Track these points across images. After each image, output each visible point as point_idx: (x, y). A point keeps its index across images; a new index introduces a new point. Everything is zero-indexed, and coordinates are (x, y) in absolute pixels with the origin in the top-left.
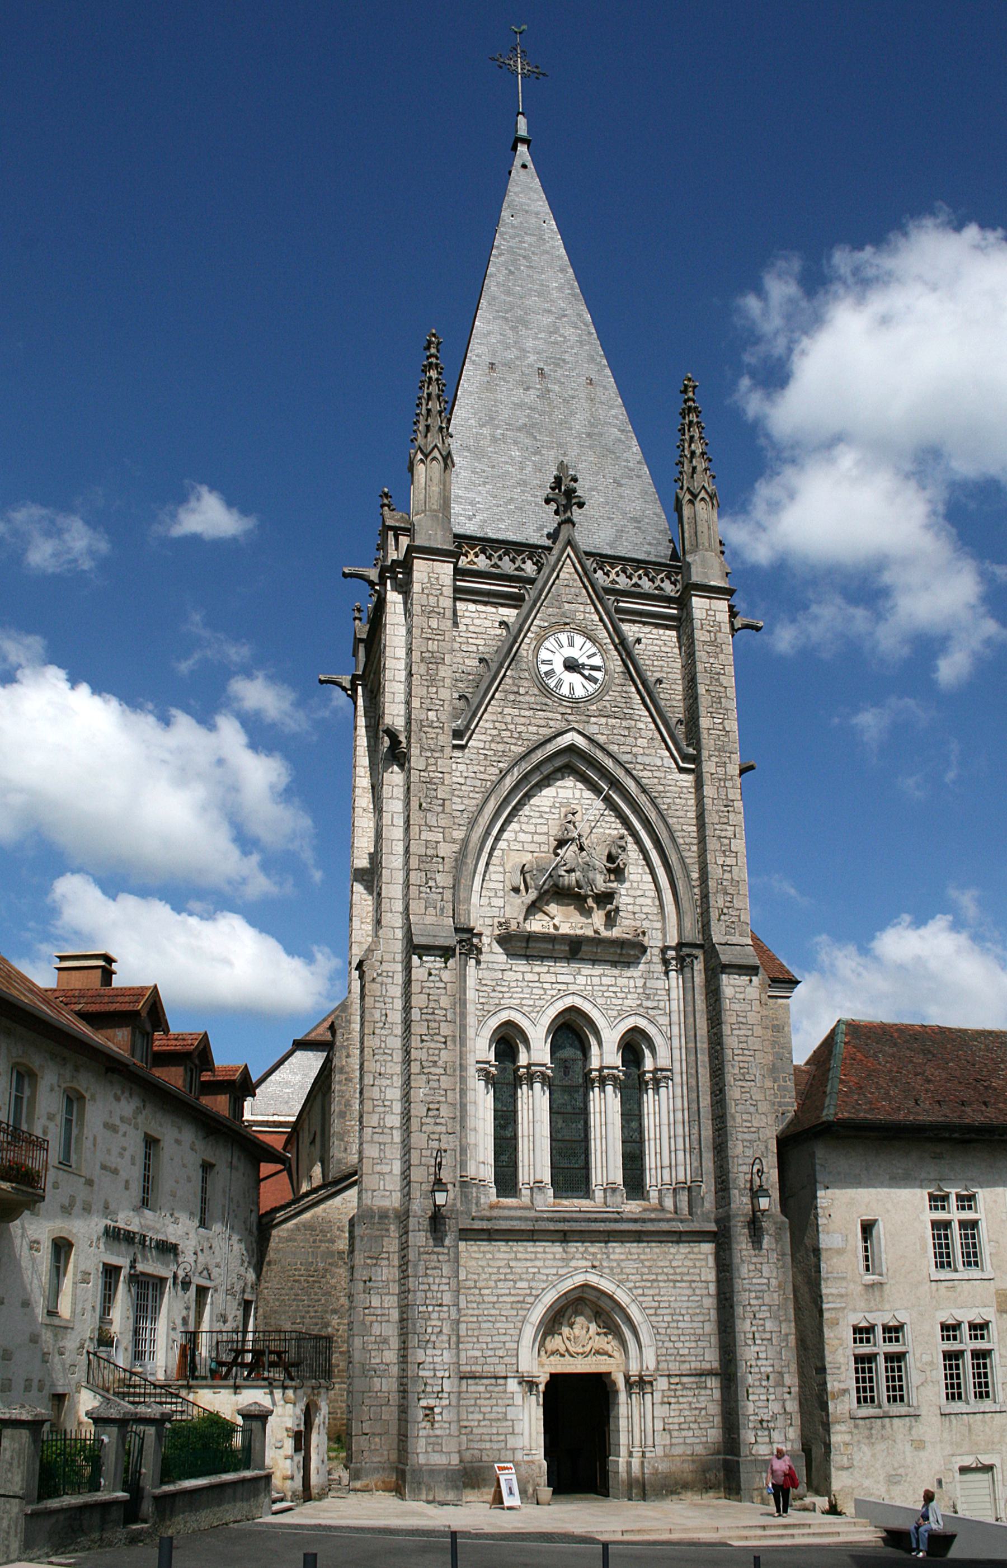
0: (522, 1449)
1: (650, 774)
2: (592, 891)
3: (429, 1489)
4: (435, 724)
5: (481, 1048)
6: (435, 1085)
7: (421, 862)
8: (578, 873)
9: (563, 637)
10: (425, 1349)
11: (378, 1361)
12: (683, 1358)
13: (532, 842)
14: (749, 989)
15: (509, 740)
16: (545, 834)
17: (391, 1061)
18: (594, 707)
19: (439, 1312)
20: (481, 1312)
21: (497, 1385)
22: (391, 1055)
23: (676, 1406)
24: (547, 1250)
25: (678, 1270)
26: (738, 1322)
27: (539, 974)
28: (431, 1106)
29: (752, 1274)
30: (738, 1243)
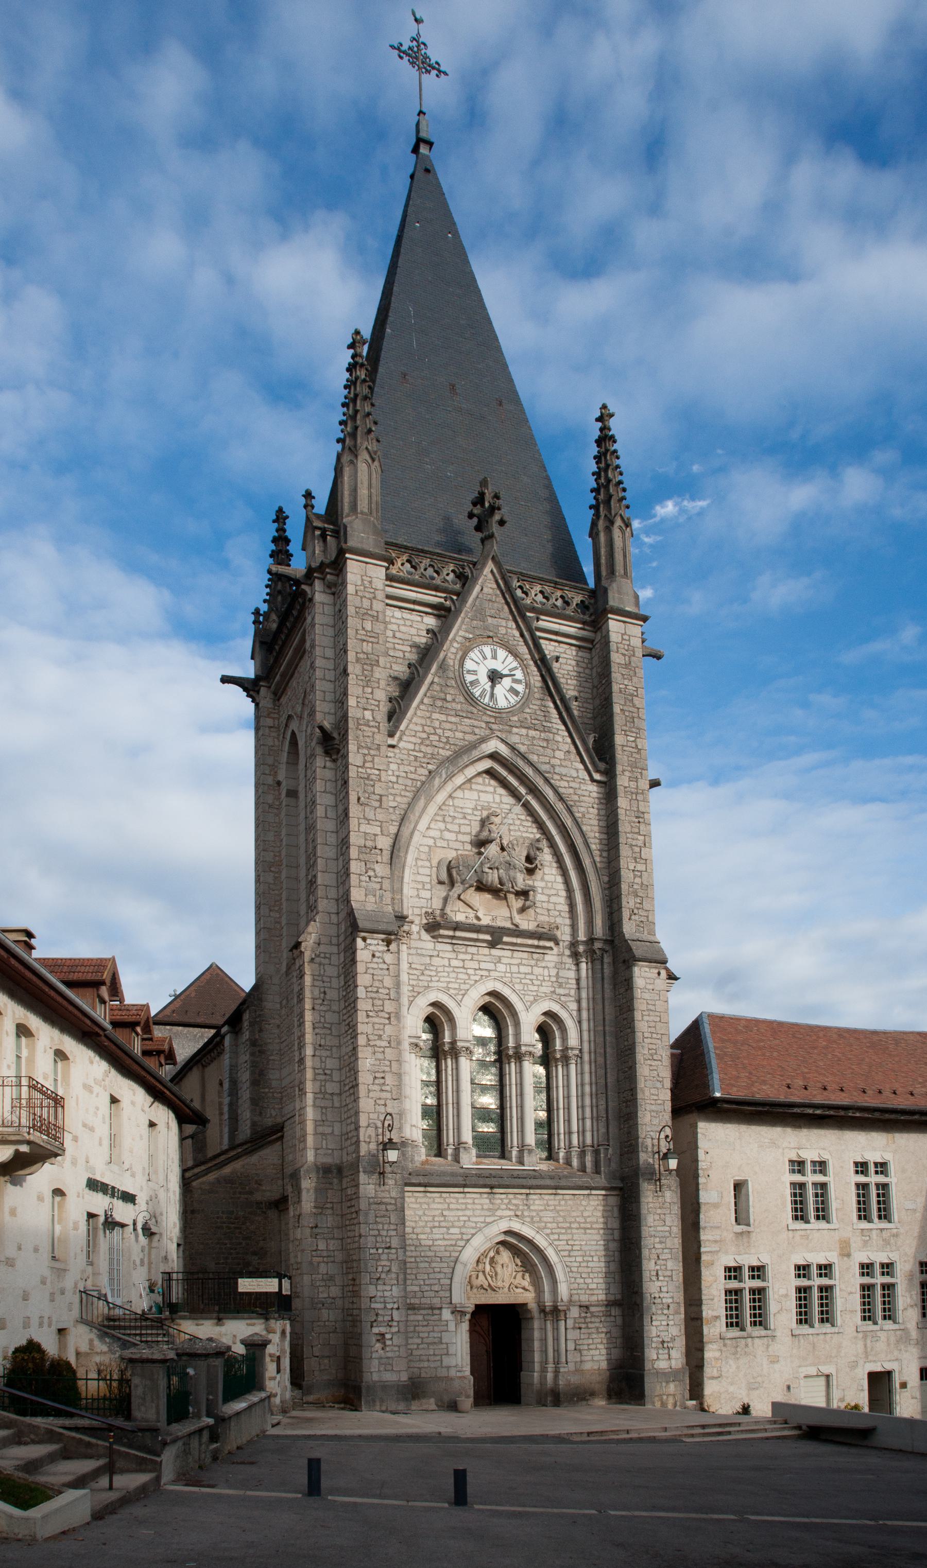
0: (456, 1366)
1: (566, 784)
2: (513, 887)
3: (382, 1401)
4: (372, 724)
5: (413, 1025)
6: (380, 1056)
7: (360, 852)
9: (487, 650)
10: (376, 1285)
11: (326, 1295)
13: (456, 840)
14: (657, 981)
16: (467, 834)
18: (516, 718)
20: (418, 1254)
21: (433, 1315)
22: (330, 1029)
24: (476, 1201)
25: (588, 1220)
26: (644, 1262)
27: (463, 961)
28: (377, 1075)
29: (656, 1223)
30: (647, 1197)
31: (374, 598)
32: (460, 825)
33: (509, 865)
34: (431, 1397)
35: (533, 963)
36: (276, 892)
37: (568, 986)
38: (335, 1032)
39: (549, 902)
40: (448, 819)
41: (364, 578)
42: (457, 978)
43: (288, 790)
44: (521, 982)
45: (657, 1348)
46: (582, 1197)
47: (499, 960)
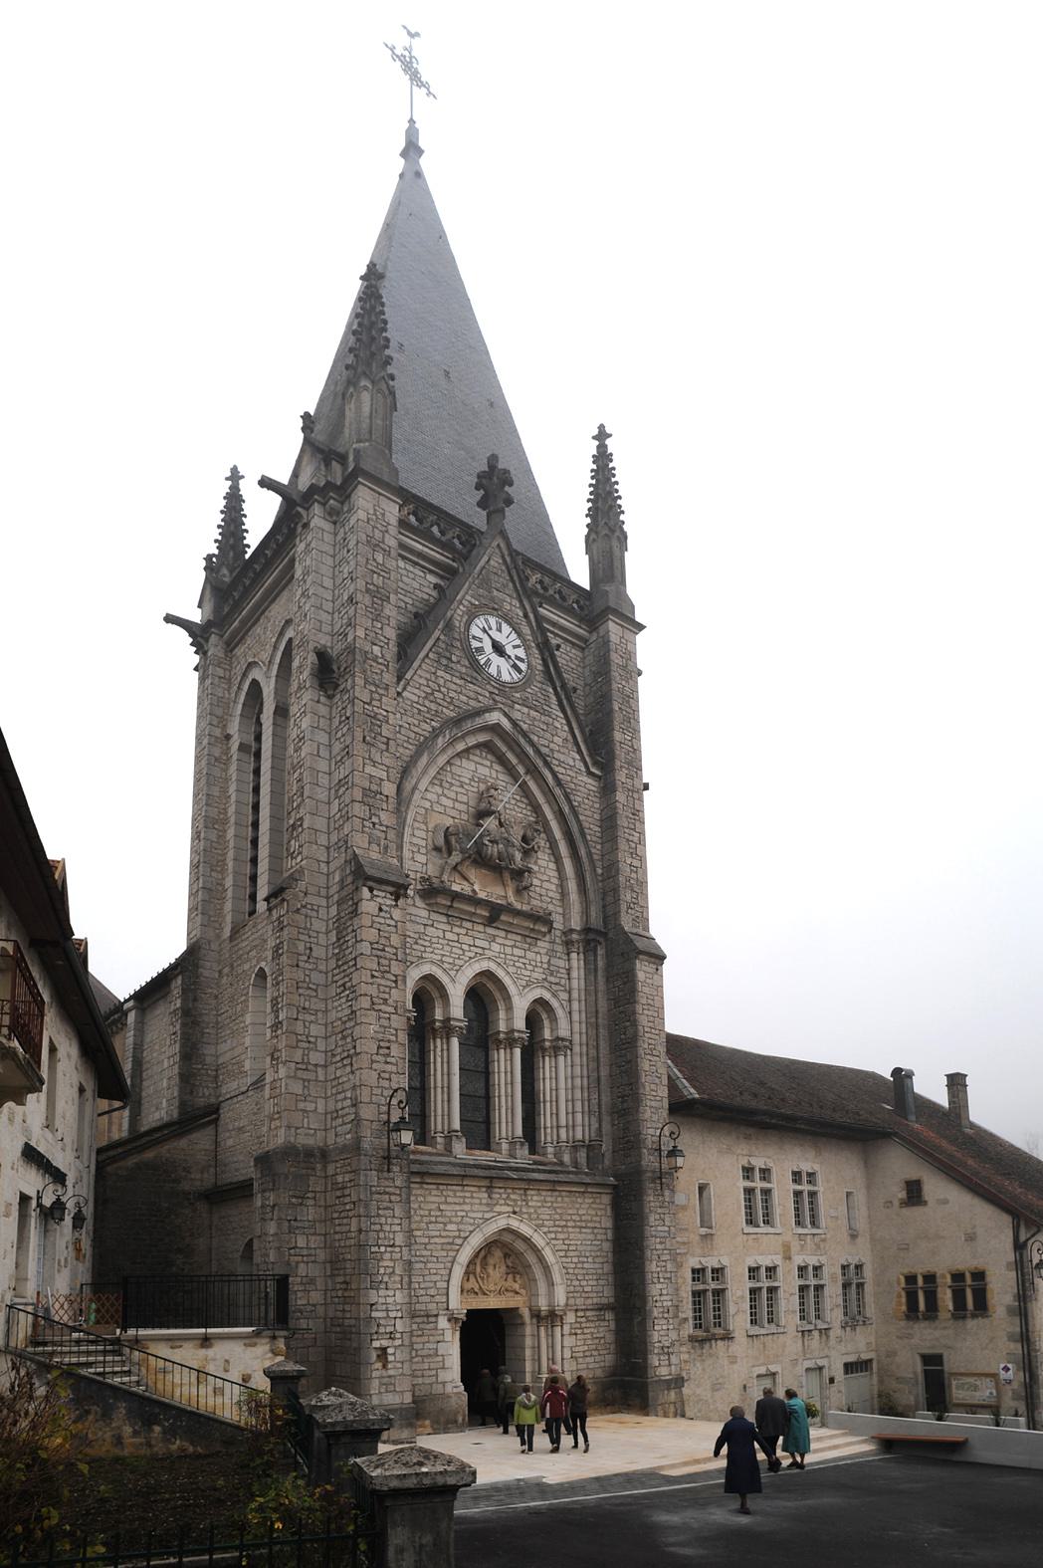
4: (380, 661)
6: (385, 1023)
10: (377, 1289)
11: (304, 1302)
12: (587, 1295)
13: (453, 808)
16: (465, 803)
17: (316, 997)
18: (518, 695)
19: (391, 1252)
21: (429, 1323)
22: (316, 991)
23: (582, 1337)
24: (474, 1195)
25: (584, 1218)
26: (648, 1263)
28: (382, 1044)
31: (387, 531)
33: (508, 842)
34: (426, 1419)
36: (220, 852)
37: (559, 975)
38: (321, 995)
40: (444, 784)
41: (377, 508)
42: (451, 953)
43: (241, 744)
44: (514, 965)
45: (659, 1354)
46: (577, 1195)
47: (493, 938)
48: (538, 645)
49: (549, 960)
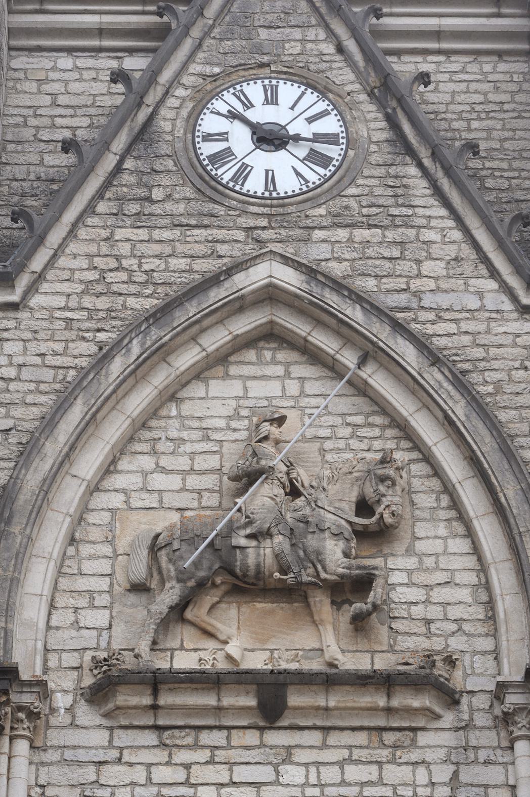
1: (452, 328)
8: (278, 539)
13: (183, 489)
15: (123, 288)
16: (212, 471)
18: (322, 211)
27: (187, 767)
32: (192, 455)
35: (385, 753)
39: (428, 602)
47: (287, 755)
48: (371, 94)
49: (456, 774)
